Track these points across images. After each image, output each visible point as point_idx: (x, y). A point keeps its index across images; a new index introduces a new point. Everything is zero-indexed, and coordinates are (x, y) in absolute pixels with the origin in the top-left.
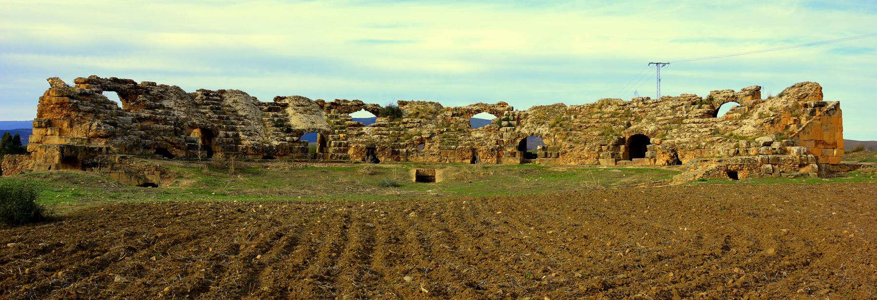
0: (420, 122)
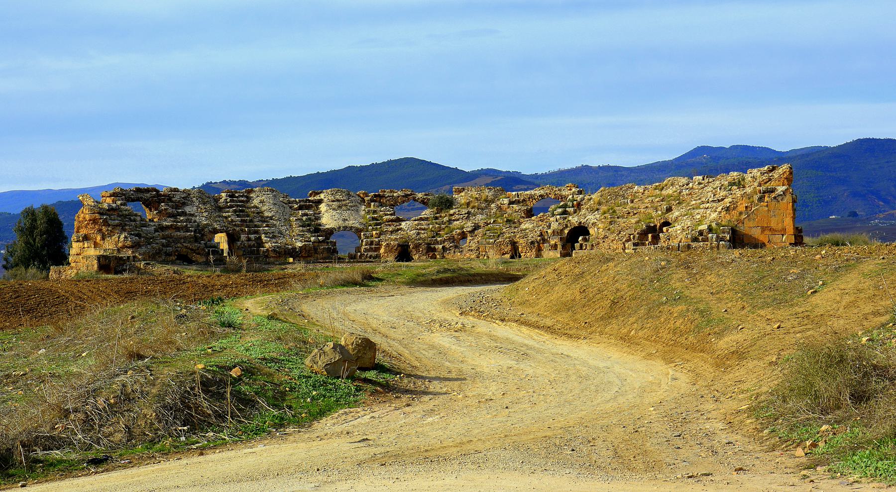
0: (469, 213)
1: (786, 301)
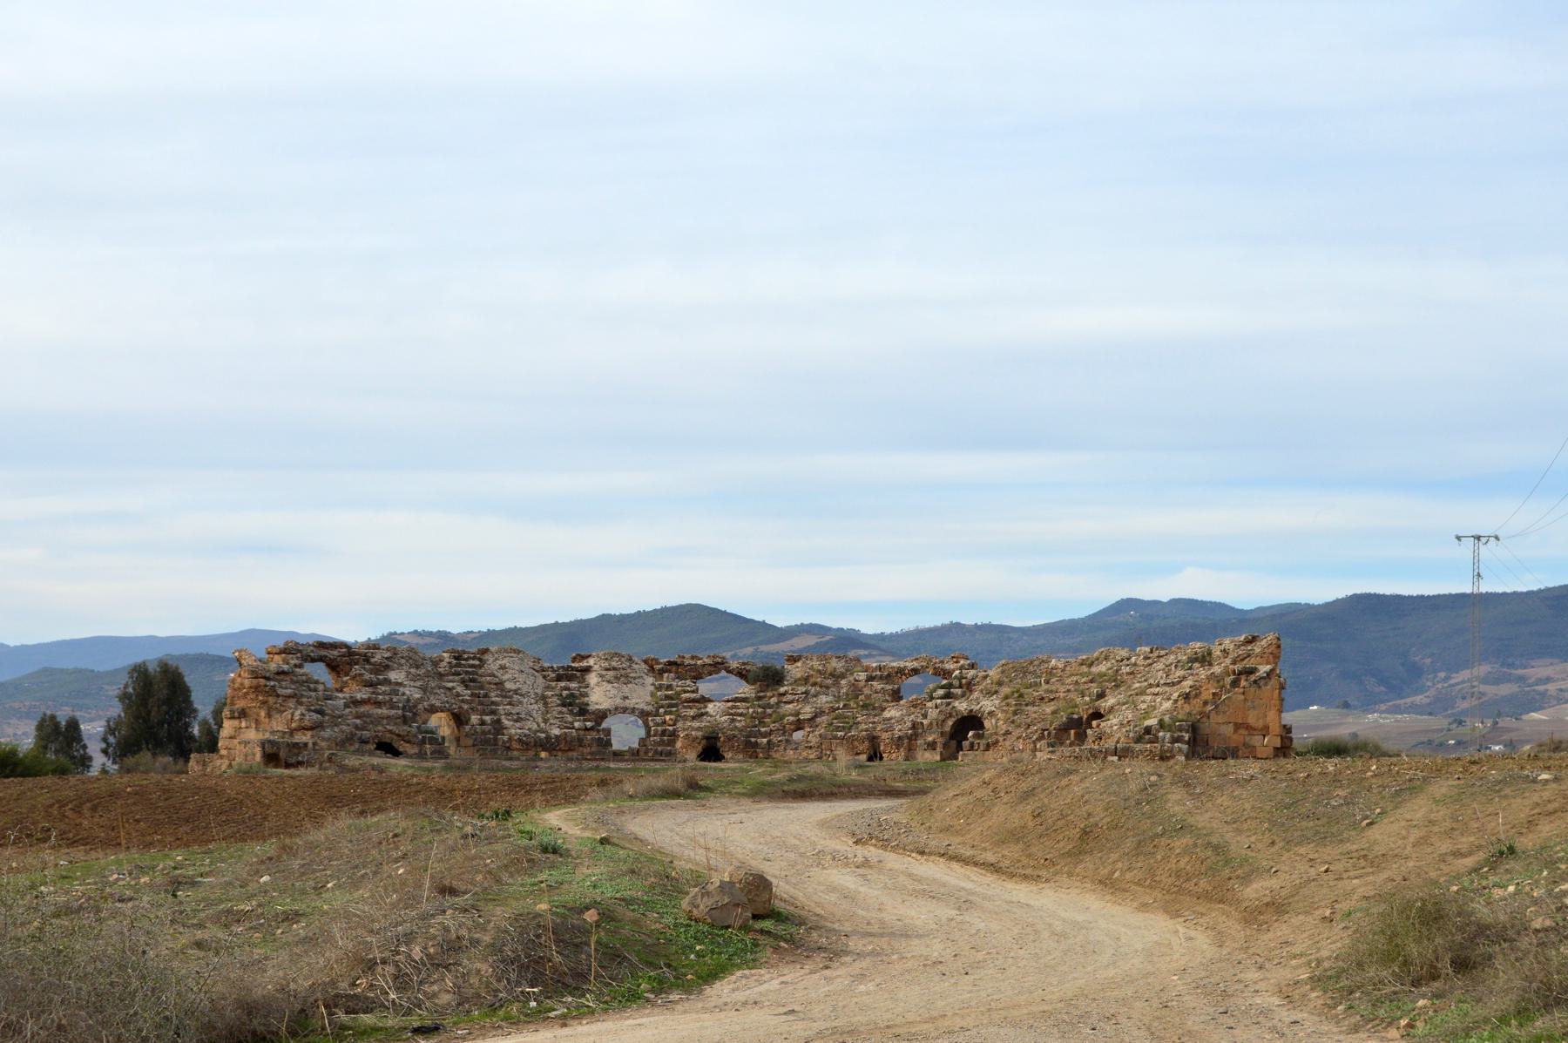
0: (806, 693)
1: (1333, 835)
